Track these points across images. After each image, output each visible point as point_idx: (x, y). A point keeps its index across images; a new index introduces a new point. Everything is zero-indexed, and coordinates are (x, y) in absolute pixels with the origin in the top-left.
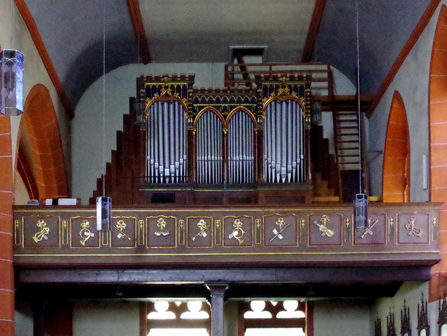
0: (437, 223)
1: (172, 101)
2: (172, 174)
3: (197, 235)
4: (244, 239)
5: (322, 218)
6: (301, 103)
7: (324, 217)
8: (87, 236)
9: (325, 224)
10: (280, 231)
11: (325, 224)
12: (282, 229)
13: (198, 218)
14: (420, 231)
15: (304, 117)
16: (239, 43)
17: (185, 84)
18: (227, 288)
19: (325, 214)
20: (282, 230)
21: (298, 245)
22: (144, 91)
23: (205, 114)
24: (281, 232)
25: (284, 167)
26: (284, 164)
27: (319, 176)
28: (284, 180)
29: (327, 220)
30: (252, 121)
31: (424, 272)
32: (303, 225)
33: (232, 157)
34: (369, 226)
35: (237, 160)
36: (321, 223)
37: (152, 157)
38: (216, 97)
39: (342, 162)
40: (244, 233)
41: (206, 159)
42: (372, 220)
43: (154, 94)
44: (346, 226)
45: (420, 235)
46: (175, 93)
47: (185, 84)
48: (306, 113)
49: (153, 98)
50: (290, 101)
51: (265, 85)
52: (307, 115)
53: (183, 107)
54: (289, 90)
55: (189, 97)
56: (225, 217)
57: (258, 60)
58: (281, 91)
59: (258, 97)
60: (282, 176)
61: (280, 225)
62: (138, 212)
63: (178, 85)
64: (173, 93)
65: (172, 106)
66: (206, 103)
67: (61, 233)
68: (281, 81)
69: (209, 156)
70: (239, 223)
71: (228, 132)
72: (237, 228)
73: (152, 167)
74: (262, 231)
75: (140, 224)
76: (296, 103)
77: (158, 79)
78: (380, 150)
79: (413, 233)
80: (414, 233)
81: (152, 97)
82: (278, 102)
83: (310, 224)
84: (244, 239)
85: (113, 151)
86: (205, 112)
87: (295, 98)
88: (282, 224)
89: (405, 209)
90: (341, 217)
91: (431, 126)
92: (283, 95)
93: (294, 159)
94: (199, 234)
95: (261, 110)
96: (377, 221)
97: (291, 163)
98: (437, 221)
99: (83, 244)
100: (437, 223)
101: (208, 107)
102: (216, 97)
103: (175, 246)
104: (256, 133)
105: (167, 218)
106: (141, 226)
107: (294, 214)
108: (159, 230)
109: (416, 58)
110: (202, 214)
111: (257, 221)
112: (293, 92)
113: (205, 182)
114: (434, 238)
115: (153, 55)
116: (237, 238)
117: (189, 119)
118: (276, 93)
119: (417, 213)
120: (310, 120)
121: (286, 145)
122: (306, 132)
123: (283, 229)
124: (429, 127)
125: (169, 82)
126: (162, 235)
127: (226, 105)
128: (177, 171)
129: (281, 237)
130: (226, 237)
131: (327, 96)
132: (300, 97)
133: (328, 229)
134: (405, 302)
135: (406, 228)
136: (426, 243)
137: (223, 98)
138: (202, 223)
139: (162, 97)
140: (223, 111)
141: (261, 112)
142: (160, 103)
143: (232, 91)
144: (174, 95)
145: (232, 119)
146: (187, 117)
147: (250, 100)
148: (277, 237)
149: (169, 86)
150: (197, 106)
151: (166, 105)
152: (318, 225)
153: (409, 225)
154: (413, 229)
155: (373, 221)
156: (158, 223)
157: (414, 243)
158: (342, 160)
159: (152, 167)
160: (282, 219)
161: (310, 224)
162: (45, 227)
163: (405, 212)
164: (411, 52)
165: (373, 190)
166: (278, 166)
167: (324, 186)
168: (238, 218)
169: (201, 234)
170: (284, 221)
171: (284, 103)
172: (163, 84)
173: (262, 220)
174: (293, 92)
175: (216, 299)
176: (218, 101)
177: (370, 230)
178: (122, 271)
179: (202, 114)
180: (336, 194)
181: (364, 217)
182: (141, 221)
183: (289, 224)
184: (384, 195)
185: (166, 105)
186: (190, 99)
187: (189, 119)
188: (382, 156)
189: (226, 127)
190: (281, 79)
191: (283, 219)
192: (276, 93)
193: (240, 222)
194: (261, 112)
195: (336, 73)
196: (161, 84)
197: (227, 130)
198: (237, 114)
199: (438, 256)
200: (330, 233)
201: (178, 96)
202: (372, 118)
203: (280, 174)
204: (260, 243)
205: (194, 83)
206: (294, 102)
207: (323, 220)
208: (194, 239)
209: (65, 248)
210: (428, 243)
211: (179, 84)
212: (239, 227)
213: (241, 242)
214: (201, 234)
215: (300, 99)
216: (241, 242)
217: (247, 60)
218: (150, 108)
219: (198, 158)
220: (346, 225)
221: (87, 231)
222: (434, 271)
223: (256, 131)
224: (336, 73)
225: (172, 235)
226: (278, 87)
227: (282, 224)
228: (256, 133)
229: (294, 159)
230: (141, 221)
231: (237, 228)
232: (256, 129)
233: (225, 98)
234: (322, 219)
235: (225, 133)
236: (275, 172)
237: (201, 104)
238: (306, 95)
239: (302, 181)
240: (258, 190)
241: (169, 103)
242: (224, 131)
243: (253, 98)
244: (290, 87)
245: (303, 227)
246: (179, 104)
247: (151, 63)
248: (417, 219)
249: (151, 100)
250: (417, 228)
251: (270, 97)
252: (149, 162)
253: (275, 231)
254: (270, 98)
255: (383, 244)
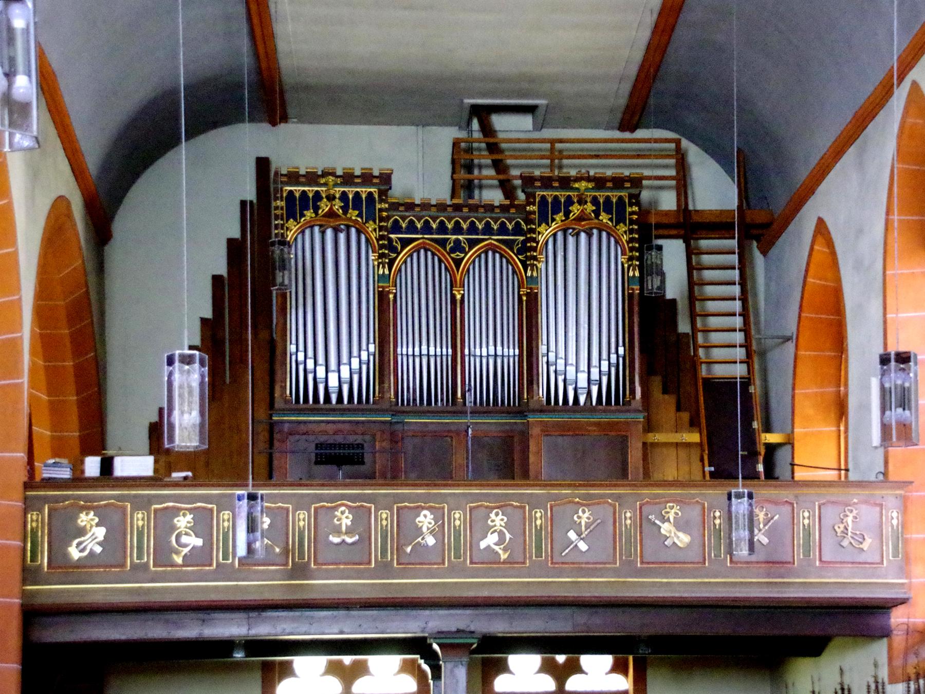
0: (900, 521)
1: (342, 227)
2: (344, 383)
3: (417, 541)
4: (509, 551)
5: (666, 508)
6: (619, 236)
7: (669, 506)
8: (185, 546)
9: (672, 520)
10: (582, 534)
11: (672, 520)
12: (586, 530)
13: (418, 507)
14: (864, 539)
15: (626, 265)
16: (484, 95)
17: (372, 190)
18: (475, 646)
19: (673, 502)
20: (586, 533)
21: (618, 564)
22: (283, 204)
23: (415, 255)
24: (583, 536)
25: (584, 371)
26: (583, 366)
27: (656, 383)
28: (582, 399)
29: (676, 514)
30: (514, 272)
31: (875, 621)
32: (628, 522)
33: (472, 349)
34: (761, 526)
35: (483, 355)
36: (664, 520)
37: (301, 347)
38: (438, 221)
39: (705, 344)
40: (510, 538)
41: (417, 352)
42: (766, 514)
43: (305, 212)
44: (715, 525)
45: (865, 546)
46: (350, 211)
47: (372, 190)
48: (631, 259)
49: (303, 219)
50: (595, 231)
51: (543, 197)
52: (632, 263)
53: (367, 240)
54: (594, 208)
55: (382, 219)
56: (471, 505)
57: (525, 122)
58: (576, 209)
59: (528, 221)
60: (579, 391)
61: (583, 524)
62: (295, 494)
63: (357, 193)
64: (345, 209)
65: (342, 237)
66: (417, 234)
67: (132, 540)
68: (578, 189)
69: (424, 347)
70: (500, 517)
71: (463, 296)
72: (495, 528)
73: (301, 367)
74: (546, 532)
75: (299, 520)
76: (609, 235)
77: (312, 178)
78: (788, 334)
79: (851, 543)
80: (852, 541)
81: (300, 219)
82: (570, 234)
83: (642, 521)
84: (509, 551)
85: (204, 321)
86: (414, 251)
87: (606, 225)
88: (587, 521)
89: (835, 494)
90: (704, 508)
91: (889, 321)
92: (580, 218)
93: (605, 355)
94: (420, 539)
95: (535, 249)
96: (776, 517)
97: (598, 365)
98: (900, 518)
99: (179, 560)
100: (900, 521)
101: (421, 241)
102: (438, 221)
103: (369, 563)
104: (524, 298)
105: (355, 507)
106: (302, 523)
107: (610, 501)
108: (337, 531)
109: (860, 165)
110: (427, 498)
111: (536, 512)
112: (603, 214)
113: (414, 400)
114: (893, 553)
115: (291, 111)
116: (497, 548)
117: (381, 266)
118: (567, 214)
119: (859, 501)
120: (637, 274)
121: (586, 326)
122: (629, 299)
123: (589, 530)
124: (885, 322)
125: (336, 185)
126: (343, 541)
127: (460, 237)
128: (356, 378)
129: (583, 546)
130: (473, 546)
131: (675, 211)
132: (616, 225)
133: (679, 531)
134: (841, 671)
135: (837, 532)
136: (877, 563)
137: (453, 222)
138: (425, 520)
139: (321, 218)
140: (453, 250)
141: (535, 254)
142: (316, 229)
143: (474, 208)
144: (349, 215)
145: (471, 268)
146: (376, 263)
147: (510, 227)
148: (576, 545)
149: (337, 196)
150: (397, 238)
151: (329, 233)
152: (657, 522)
153: (842, 526)
154: (850, 534)
155: (769, 516)
156: (336, 516)
157: (853, 563)
158: (706, 339)
159: (301, 367)
160: (587, 510)
161: (642, 521)
162: (98, 525)
163: (833, 499)
164: (852, 151)
165: (775, 417)
166: (571, 370)
167: (666, 406)
168: (498, 508)
169: (423, 539)
170: (590, 515)
171: (583, 236)
172: (324, 189)
173: (546, 513)
174: (603, 214)
175: (452, 671)
176: (442, 229)
177: (763, 534)
178: (257, 613)
179: (408, 256)
180: (694, 424)
181: (747, 533)
182: (302, 514)
183: (599, 521)
184: (796, 430)
185: (329, 233)
186: (382, 224)
187: (381, 266)
188: (791, 346)
189: (460, 284)
190: (576, 185)
191: (589, 511)
192: (567, 214)
193: (502, 515)
194: (535, 254)
195: (694, 153)
196: (319, 189)
197: (462, 292)
198: (483, 256)
199: (903, 591)
200: (683, 539)
201: (357, 216)
202: (774, 251)
203: (574, 386)
204: (542, 557)
205: (390, 188)
206: (604, 234)
207: (668, 513)
208: (409, 549)
209: (140, 570)
210: (882, 563)
211: (358, 190)
212: (501, 526)
213: (504, 556)
214: (423, 539)
215: (618, 227)
216: (504, 556)
217: (500, 122)
218: (296, 239)
219: (399, 350)
220: (714, 523)
221: (186, 534)
222: (897, 617)
223: (524, 294)
224: (694, 153)
225: (365, 539)
226: (569, 202)
227: (587, 521)
228: (524, 298)
229: (605, 355)
230: (302, 512)
231: (495, 528)
232: (523, 291)
233: (457, 223)
234: (666, 510)
235: (459, 297)
236: (565, 380)
237: (406, 233)
238: (629, 219)
239: (621, 403)
240: (528, 421)
241: (336, 230)
242: (456, 293)
243: (518, 224)
244: (595, 201)
245: (628, 527)
246: (359, 232)
247: (286, 122)
248: (857, 514)
249: (298, 223)
250: (858, 533)
251: (554, 224)
252: (294, 357)
253: (572, 535)
254: (554, 225)
255: (789, 563)
